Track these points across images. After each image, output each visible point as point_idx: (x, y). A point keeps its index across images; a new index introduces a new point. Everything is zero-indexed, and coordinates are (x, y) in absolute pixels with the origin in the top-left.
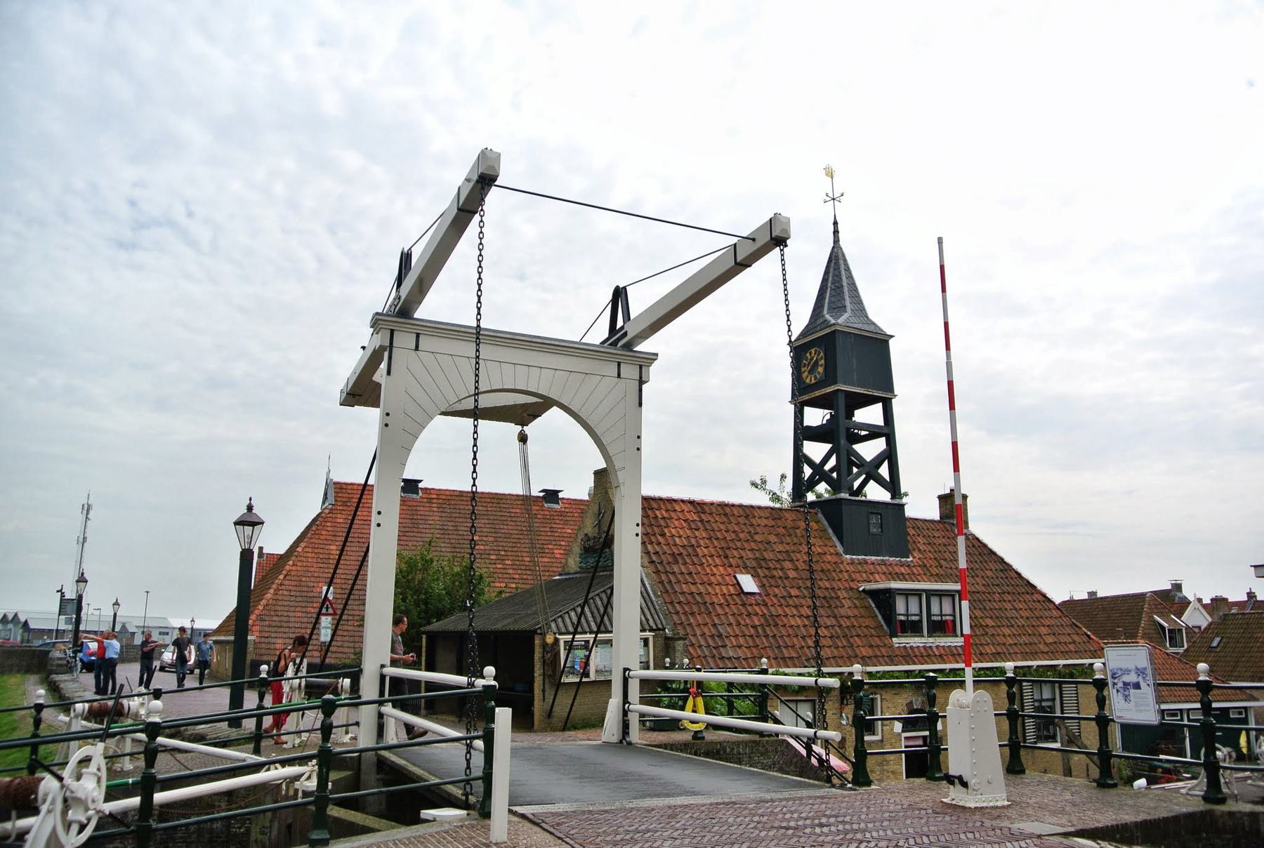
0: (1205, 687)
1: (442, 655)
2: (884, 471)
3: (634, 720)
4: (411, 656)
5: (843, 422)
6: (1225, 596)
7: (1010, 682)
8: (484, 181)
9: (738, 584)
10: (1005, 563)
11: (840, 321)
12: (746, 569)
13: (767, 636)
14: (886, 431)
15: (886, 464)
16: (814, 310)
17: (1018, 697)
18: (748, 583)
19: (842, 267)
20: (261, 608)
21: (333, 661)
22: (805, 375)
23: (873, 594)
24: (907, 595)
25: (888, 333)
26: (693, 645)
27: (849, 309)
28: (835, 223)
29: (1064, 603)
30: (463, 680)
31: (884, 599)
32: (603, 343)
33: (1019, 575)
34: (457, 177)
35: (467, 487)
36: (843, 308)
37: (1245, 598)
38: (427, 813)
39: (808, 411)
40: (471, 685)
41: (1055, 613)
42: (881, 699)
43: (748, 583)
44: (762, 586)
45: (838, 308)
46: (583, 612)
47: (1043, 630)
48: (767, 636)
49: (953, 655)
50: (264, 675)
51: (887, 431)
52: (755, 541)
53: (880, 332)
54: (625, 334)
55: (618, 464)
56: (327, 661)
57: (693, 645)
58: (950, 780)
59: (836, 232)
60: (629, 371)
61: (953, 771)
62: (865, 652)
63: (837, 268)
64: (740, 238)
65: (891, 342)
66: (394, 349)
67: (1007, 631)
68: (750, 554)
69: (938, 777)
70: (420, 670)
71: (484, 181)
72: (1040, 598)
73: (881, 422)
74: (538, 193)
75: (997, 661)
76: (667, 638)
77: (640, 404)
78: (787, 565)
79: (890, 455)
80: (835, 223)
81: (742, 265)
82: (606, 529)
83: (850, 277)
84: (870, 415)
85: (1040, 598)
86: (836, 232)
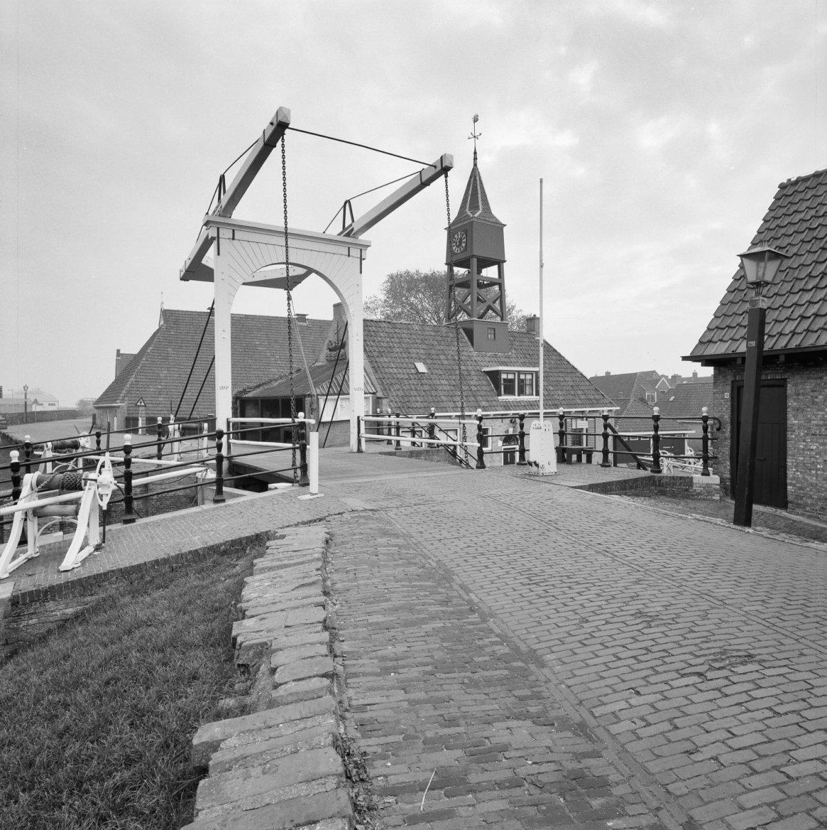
0: (656, 418)
1: (249, 409)
2: (497, 305)
3: (363, 440)
4: (522, 377)
5: (476, 277)
6: (679, 374)
7: (561, 417)
8: (280, 128)
9: (416, 367)
10: (562, 356)
11: (476, 215)
12: (420, 360)
13: (432, 396)
14: (498, 282)
15: (498, 302)
16: (461, 208)
17: (564, 426)
18: (421, 368)
19: (478, 182)
20: (128, 386)
21: (182, 416)
22: (454, 248)
23: (488, 373)
24: (525, 374)
25: (503, 223)
26: (392, 401)
27: (481, 208)
28: (475, 153)
29: (592, 378)
30: (289, 420)
31: (494, 376)
32: (339, 234)
33: (568, 362)
34: (260, 127)
35: (285, 315)
36: (477, 208)
37: (691, 376)
38: (270, 486)
39: (456, 269)
40: (294, 422)
41: (587, 383)
42: (492, 429)
43: (421, 368)
44: (429, 369)
45: (474, 207)
46: (330, 385)
47: (580, 392)
48: (432, 396)
49: (531, 405)
50: (160, 422)
51: (500, 283)
52: (425, 344)
53: (498, 222)
54: (353, 230)
55: (348, 301)
56: (325, 397)
57: (392, 401)
58: (530, 464)
59: (475, 159)
60: (355, 252)
61: (532, 460)
62: (484, 404)
63: (475, 180)
64: (426, 167)
65: (505, 228)
66: (220, 239)
67: (560, 393)
68: (422, 351)
69: (707, 444)
70: (238, 417)
71: (280, 128)
72: (579, 376)
73: (496, 276)
74: (317, 133)
75: (517, 410)
76: (378, 398)
77: (361, 272)
78: (442, 357)
79: (501, 297)
80: (475, 153)
81: (424, 184)
82: (341, 338)
83: (482, 188)
84: (490, 272)
85: (579, 376)
86: (475, 159)
